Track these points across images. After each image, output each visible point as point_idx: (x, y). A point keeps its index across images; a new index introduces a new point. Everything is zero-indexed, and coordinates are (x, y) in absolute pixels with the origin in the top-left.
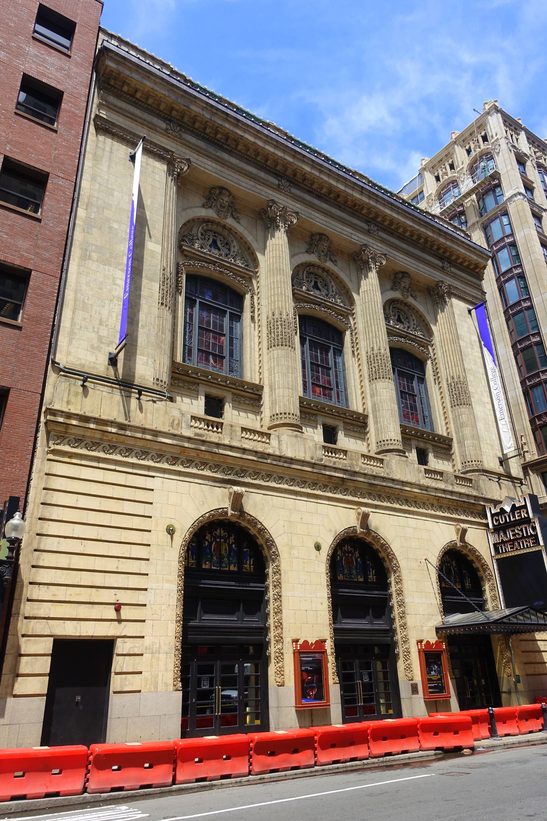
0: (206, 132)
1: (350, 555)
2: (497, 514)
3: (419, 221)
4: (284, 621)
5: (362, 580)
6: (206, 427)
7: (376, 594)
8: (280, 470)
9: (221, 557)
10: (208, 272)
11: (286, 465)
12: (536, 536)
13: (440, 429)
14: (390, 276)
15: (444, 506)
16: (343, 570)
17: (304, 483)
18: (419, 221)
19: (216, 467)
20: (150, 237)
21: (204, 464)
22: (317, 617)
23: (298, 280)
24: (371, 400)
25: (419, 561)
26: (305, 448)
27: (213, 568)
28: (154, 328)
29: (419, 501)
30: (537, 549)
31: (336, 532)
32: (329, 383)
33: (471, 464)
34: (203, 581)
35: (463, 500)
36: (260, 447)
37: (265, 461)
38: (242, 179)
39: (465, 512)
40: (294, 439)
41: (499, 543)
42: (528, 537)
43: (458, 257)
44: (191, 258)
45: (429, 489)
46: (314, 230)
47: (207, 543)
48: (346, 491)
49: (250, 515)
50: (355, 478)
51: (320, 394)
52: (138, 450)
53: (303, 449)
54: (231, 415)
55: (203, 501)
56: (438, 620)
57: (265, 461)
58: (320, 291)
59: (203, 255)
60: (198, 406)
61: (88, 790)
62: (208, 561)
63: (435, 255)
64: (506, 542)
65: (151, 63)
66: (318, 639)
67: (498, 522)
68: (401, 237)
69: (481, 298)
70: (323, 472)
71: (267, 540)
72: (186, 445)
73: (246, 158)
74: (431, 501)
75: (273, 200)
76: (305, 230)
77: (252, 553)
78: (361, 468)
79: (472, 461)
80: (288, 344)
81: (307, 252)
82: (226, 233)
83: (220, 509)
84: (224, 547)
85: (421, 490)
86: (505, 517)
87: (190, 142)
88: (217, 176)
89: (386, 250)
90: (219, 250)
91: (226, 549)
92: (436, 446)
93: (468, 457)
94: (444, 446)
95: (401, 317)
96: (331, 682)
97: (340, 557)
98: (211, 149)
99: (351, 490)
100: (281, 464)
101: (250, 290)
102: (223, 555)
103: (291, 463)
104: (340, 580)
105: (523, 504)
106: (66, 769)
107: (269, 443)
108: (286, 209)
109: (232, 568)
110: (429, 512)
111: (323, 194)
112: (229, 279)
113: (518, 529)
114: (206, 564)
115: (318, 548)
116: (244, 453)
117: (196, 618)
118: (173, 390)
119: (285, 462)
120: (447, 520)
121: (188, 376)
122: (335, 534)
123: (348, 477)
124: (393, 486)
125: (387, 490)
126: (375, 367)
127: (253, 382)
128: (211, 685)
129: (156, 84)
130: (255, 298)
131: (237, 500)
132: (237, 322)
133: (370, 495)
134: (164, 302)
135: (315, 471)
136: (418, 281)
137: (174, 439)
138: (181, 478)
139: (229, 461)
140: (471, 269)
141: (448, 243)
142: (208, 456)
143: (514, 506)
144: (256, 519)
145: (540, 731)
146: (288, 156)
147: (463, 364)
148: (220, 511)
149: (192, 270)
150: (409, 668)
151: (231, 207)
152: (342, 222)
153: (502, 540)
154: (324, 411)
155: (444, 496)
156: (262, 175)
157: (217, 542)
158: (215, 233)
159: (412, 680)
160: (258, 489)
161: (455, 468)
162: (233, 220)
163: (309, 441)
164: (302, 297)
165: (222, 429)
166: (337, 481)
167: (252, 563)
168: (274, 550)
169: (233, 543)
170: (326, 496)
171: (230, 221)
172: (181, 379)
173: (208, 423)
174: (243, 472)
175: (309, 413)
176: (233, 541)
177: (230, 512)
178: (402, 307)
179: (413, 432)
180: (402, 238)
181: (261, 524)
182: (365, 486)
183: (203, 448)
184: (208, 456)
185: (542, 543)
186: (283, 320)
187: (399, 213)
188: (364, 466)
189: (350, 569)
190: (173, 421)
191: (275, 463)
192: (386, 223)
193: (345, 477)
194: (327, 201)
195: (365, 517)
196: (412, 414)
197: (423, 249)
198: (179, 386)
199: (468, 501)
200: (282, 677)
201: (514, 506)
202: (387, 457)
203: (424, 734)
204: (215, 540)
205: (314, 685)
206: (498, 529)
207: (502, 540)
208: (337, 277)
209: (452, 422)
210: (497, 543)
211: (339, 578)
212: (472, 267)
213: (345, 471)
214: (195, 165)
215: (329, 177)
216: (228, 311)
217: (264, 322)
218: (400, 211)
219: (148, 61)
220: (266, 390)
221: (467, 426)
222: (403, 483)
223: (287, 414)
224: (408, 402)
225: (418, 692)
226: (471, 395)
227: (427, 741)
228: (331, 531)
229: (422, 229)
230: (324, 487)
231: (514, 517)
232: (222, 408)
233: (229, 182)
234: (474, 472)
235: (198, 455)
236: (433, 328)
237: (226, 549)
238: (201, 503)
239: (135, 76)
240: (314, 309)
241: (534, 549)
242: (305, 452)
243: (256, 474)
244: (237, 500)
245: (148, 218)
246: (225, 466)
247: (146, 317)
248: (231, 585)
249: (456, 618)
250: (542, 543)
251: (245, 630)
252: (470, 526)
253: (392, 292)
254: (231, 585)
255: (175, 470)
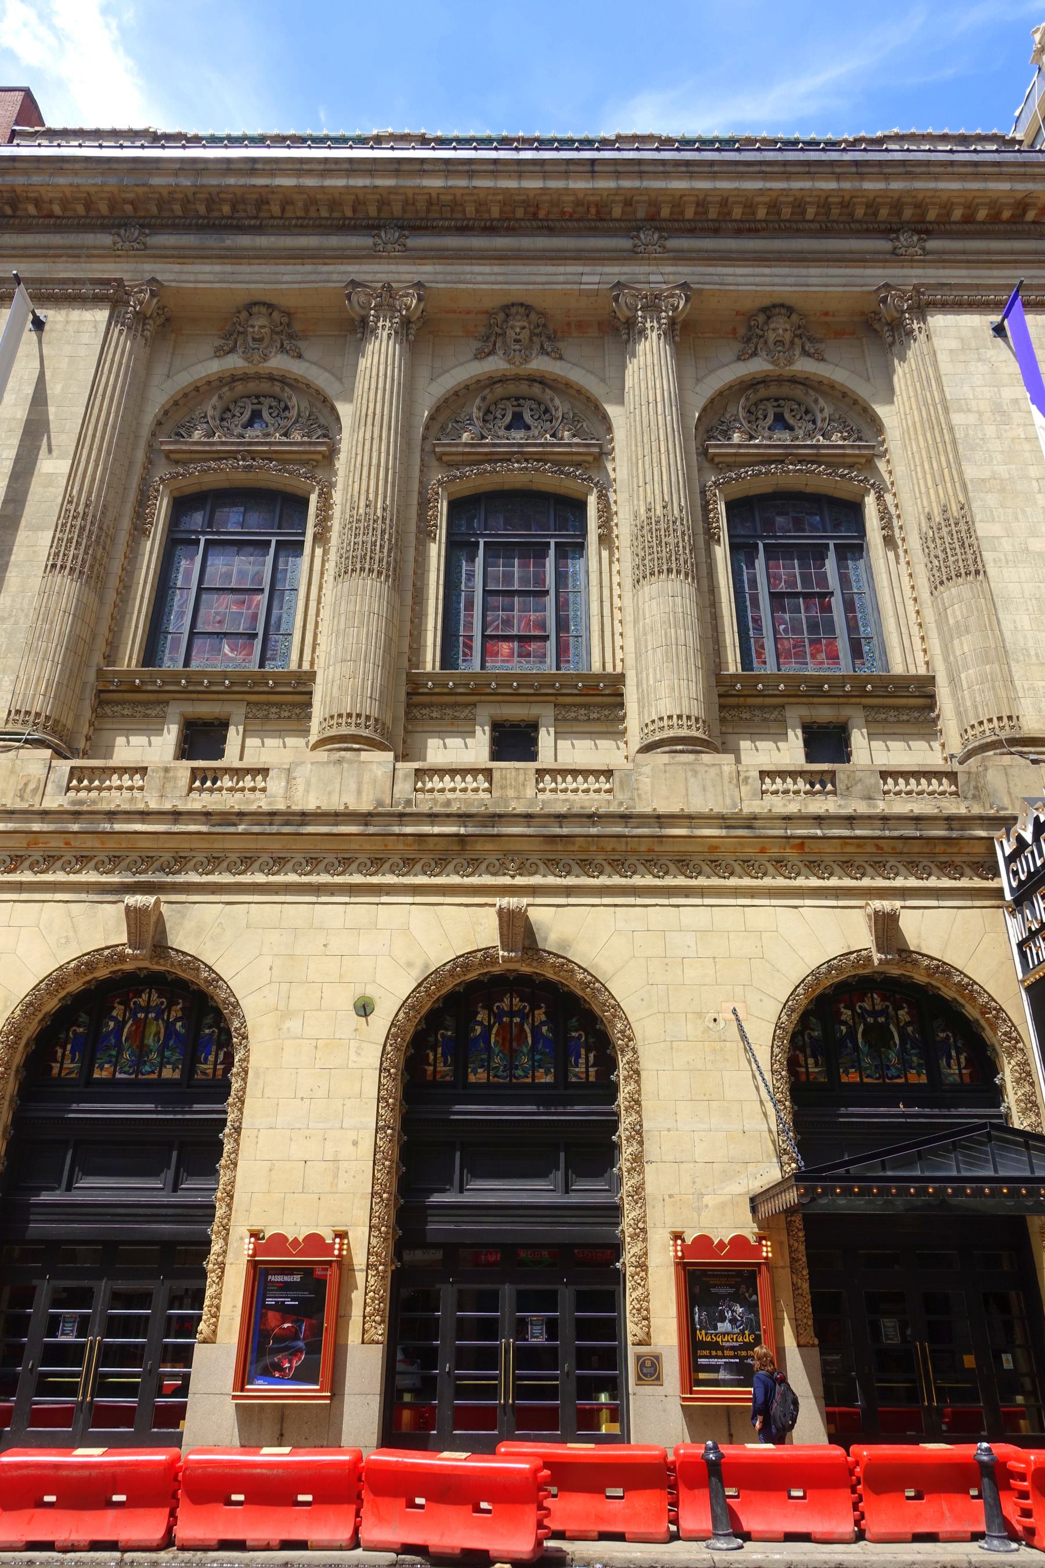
0: (783, 217)
1: (517, 1020)
3: (782, 169)
6: (808, 787)
7: (578, 1112)
8: (275, 845)
9: (142, 1052)
10: (221, 476)
11: (286, 829)
14: (734, 331)
15: (828, 859)
17: (346, 863)
18: (782, 169)
19: (115, 861)
20: (50, 451)
21: (83, 860)
22: (336, 1176)
26: (360, 784)
27: (118, 1076)
28: (27, 616)
29: (729, 858)
31: (427, 966)
32: (542, 626)
33: (978, 729)
34: (74, 1106)
35: (896, 833)
37: (232, 829)
38: (282, 268)
39: (913, 867)
40: (332, 769)
43: (947, 207)
44: (730, 467)
45: (757, 823)
46: (488, 304)
47: (844, 1028)
48: (474, 865)
49: (183, 953)
50: (495, 831)
52: (233, 857)
53: (353, 786)
54: (868, 751)
55: (67, 937)
57: (232, 829)
59: (207, 448)
60: (790, 751)
61: (867, 1535)
62: (109, 1062)
63: (867, 231)
65: (979, 148)
68: (747, 228)
70: (396, 829)
71: (984, 1010)
72: (36, 827)
73: (296, 226)
74: (774, 851)
75: (352, 281)
76: (468, 313)
77: (591, 1040)
79: (981, 723)
80: (972, 569)
81: (739, 359)
82: (277, 388)
83: (107, 948)
84: (154, 1029)
85: (728, 827)
87: (165, 248)
88: (224, 285)
89: (693, 274)
90: (791, 429)
91: (157, 1034)
92: (872, 707)
93: (971, 713)
94: (909, 704)
96: (354, 1336)
97: (849, 1027)
98: (211, 241)
99: (492, 859)
100: (274, 829)
101: (872, 485)
102: (148, 1046)
103: (303, 824)
106: (931, 1492)
107: (264, 790)
108: (390, 286)
109: (168, 1073)
110: (866, 882)
111: (498, 220)
112: (821, 480)
114: (102, 1068)
115: (364, 1009)
116: (176, 822)
117: (452, 1184)
118: (730, 730)
119: (287, 823)
120: (837, 897)
121: (137, 690)
122: (423, 972)
123: (471, 830)
124: (626, 831)
125: (609, 845)
126: (936, 557)
127: (913, 671)
128: (552, 1334)
129: (76, 174)
130: (888, 497)
131: (886, 927)
132: (854, 559)
133: (553, 865)
134: (674, 566)
135: (371, 830)
136: (826, 314)
137: (10, 821)
138: (24, 896)
139: (144, 843)
140: (1008, 222)
141: (896, 185)
142: (90, 842)
144: (945, 963)
145: (976, 1537)
146: (383, 177)
147: (961, 473)
148: (106, 952)
149: (738, 490)
151: (800, 336)
152: (552, 259)
154: (488, 691)
155: (819, 832)
156: (334, 241)
157: (866, 1024)
158: (776, 400)
160: (213, 893)
162: (810, 359)
163: (374, 767)
164: (460, 458)
165: (834, 785)
166: (443, 844)
167: (963, 1065)
168: (1005, 1029)
169: (177, 1019)
170: (405, 886)
171: (278, 362)
172: (734, 708)
173: (811, 778)
174: (181, 862)
175: (454, 705)
176: (180, 1014)
177: (877, 957)
178: (786, 390)
179: (782, 687)
180: (750, 230)
181: (210, 968)
182: (536, 845)
183: (75, 827)
184: (90, 842)
186: (952, 521)
187: (714, 176)
189: (512, 1055)
190: (26, 785)
191: (256, 829)
192: (689, 213)
193: (462, 831)
194: (513, 229)
197: (825, 230)
198: (432, 718)
199: (918, 834)
203: (379, 1500)
204: (134, 1014)
205: (301, 1344)
208: (568, 385)
211: (472, 1078)
212: (1006, 214)
213: (463, 817)
214: (173, 284)
215: (813, 179)
216: (831, 543)
217: (914, 542)
218: (716, 169)
219: (138, 144)
220: (942, 680)
222: (661, 819)
223: (1005, 720)
225: (658, 1378)
227: (381, 1520)
229: (796, 185)
230: (408, 864)
232: (534, 741)
233: (253, 286)
235: (67, 844)
236: (882, 411)
237: (157, 1034)
238: (63, 941)
239: (36, 179)
240: (766, 474)
242: (359, 792)
243: (214, 862)
244: (886, 927)
245: (51, 417)
246: (134, 856)
247: (13, 601)
248: (144, 1110)
251: (171, 1211)
252: (531, 900)
253: (741, 364)
254: (144, 1110)
255: (9, 883)
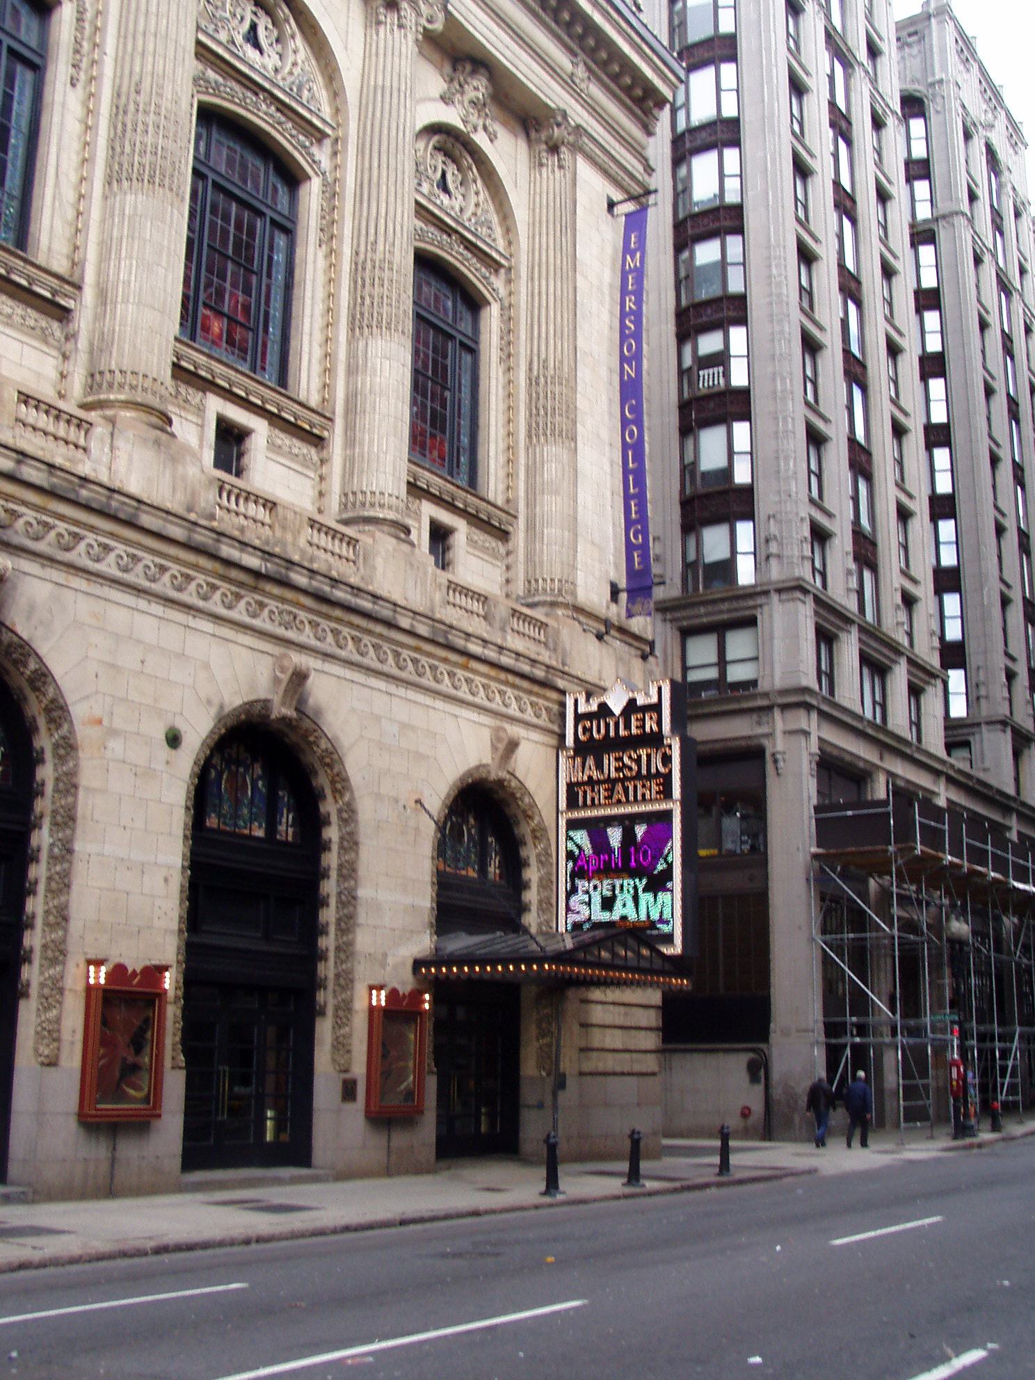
2: (589, 716)
4: (75, 912)
5: (260, 833)
12: (668, 777)
13: (492, 487)
16: (221, 806)
23: (210, 8)
24: (347, 382)
25: (402, 803)
26: (174, 477)
30: (664, 806)
31: (222, 707)
36: (59, 454)
41: (583, 783)
42: (649, 776)
51: (221, 339)
56: (424, 944)
58: (261, 52)
64: (599, 782)
66: (148, 963)
67: (588, 734)
69: (640, 178)
78: (303, 552)
86: (607, 726)
95: (449, 177)
104: (212, 830)
105: (655, 700)
113: (630, 757)
115: (174, 740)
143: (632, 702)
150: (342, 1046)
153: (590, 777)
159: (346, 1071)
161: (511, 587)
185: (677, 792)
188: (309, 550)
189: (237, 803)
195: (300, 677)
196: (433, 436)
200: (55, 1044)
201: (632, 702)
202: (368, 538)
206: (582, 749)
207: (590, 777)
209: (522, 476)
210: (579, 784)
221: (557, 493)
224: (429, 403)
226: (579, 419)
228: (209, 702)
231: (628, 726)
234: (543, 603)
241: (657, 807)
249: (460, 943)
250: (677, 792)
